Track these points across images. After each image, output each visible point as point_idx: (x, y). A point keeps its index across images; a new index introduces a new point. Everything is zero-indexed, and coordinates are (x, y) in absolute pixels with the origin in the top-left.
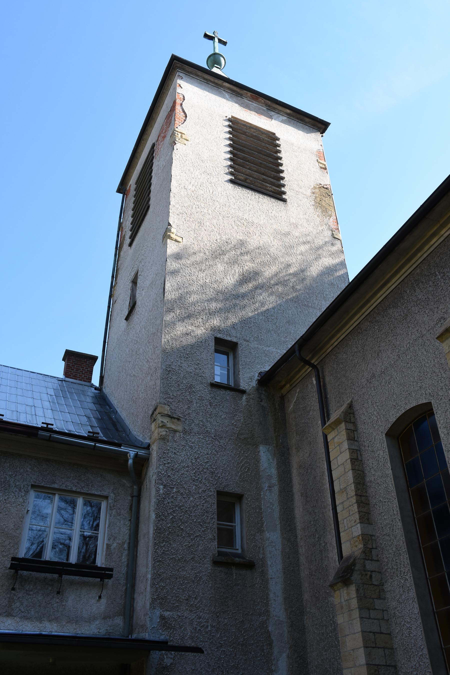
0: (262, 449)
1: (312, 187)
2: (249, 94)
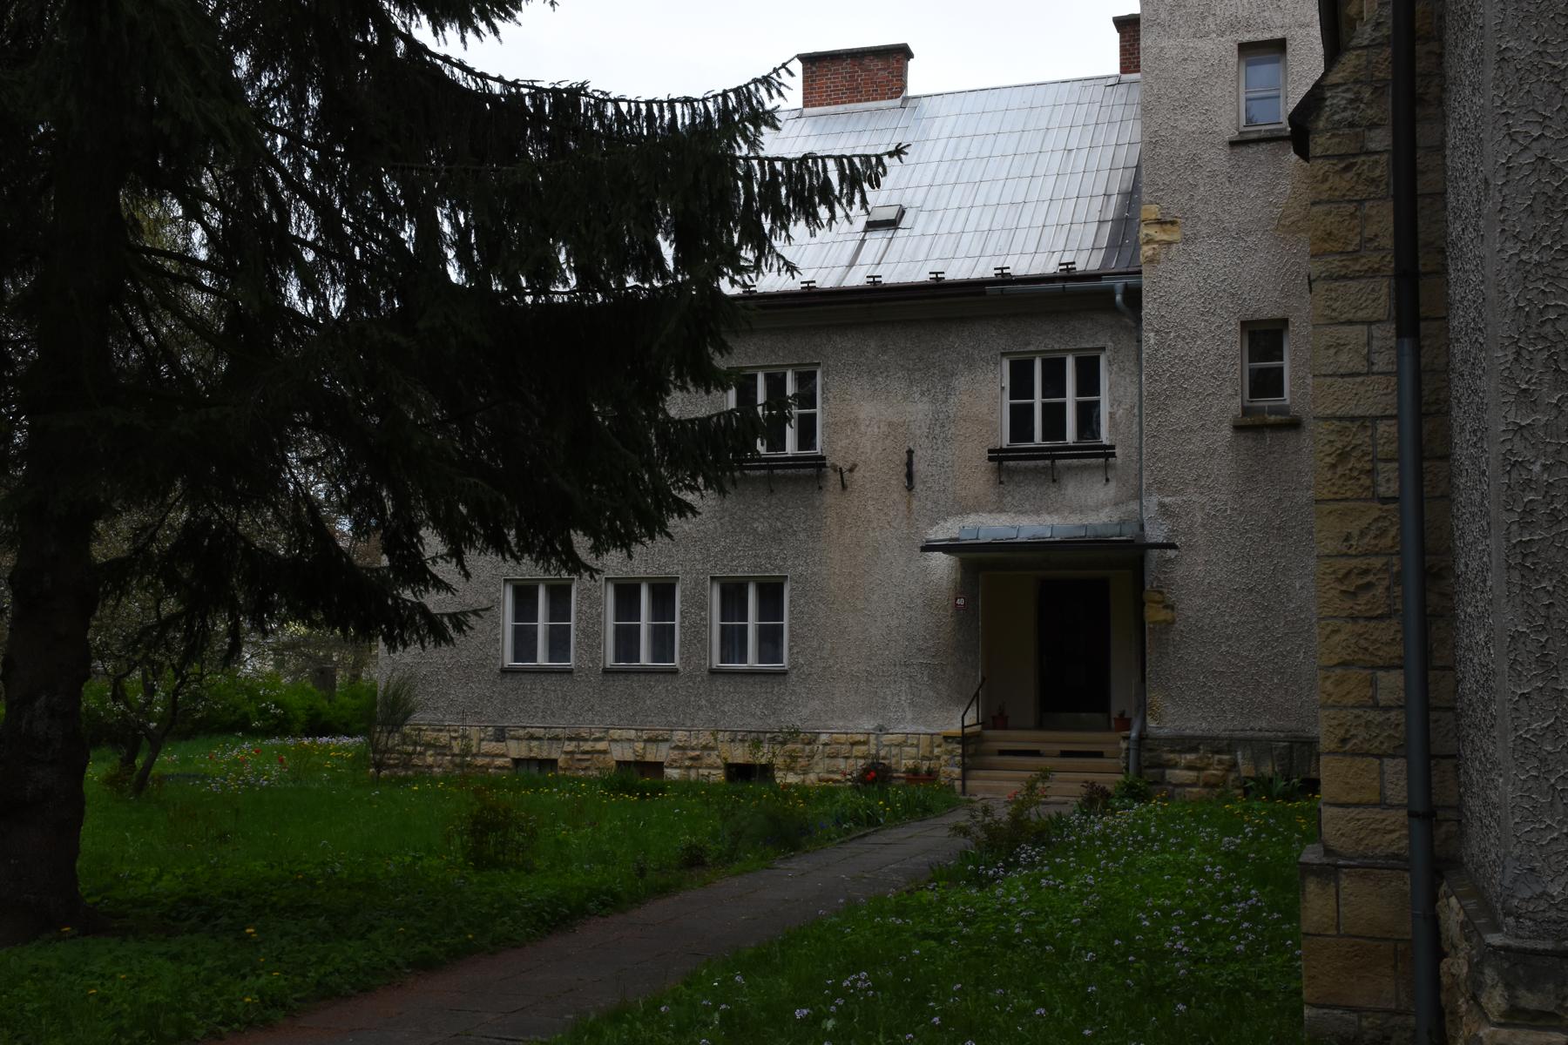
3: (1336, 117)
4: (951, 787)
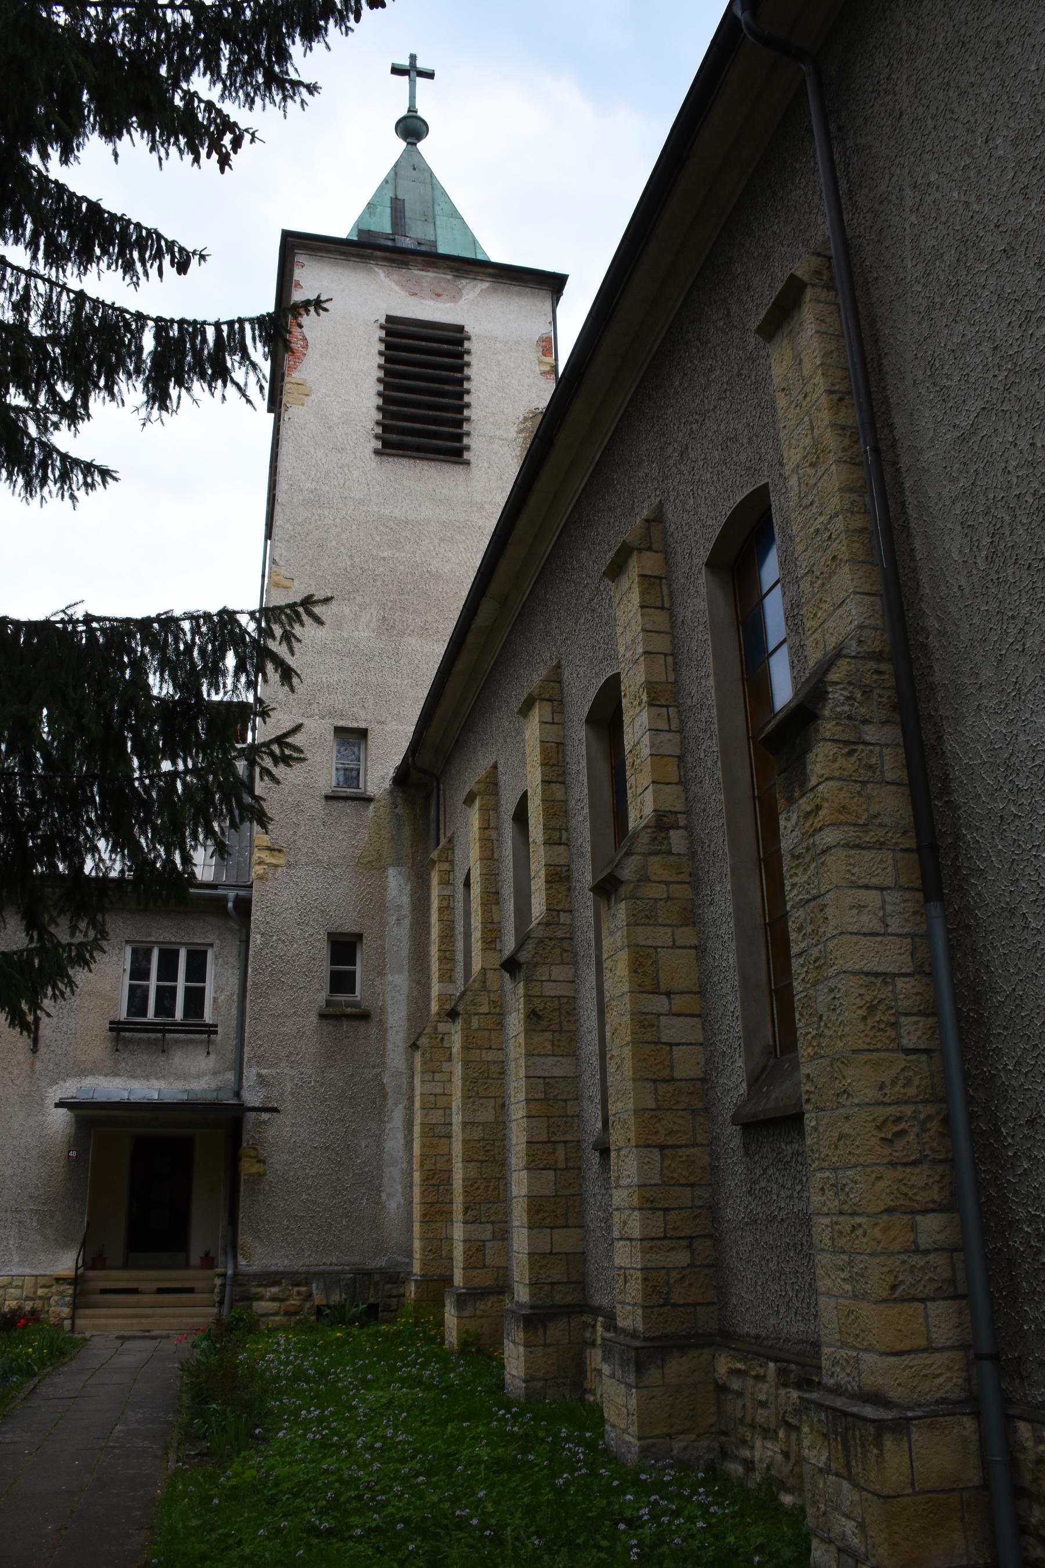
0: (391, 872)
1: (521, 418)
2: (420, 259)
3: (838, 709)
4: (59, 1326)
